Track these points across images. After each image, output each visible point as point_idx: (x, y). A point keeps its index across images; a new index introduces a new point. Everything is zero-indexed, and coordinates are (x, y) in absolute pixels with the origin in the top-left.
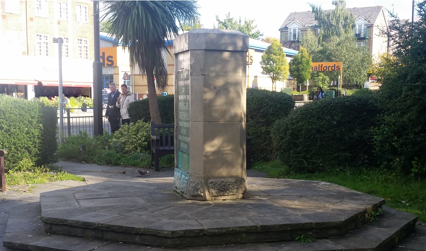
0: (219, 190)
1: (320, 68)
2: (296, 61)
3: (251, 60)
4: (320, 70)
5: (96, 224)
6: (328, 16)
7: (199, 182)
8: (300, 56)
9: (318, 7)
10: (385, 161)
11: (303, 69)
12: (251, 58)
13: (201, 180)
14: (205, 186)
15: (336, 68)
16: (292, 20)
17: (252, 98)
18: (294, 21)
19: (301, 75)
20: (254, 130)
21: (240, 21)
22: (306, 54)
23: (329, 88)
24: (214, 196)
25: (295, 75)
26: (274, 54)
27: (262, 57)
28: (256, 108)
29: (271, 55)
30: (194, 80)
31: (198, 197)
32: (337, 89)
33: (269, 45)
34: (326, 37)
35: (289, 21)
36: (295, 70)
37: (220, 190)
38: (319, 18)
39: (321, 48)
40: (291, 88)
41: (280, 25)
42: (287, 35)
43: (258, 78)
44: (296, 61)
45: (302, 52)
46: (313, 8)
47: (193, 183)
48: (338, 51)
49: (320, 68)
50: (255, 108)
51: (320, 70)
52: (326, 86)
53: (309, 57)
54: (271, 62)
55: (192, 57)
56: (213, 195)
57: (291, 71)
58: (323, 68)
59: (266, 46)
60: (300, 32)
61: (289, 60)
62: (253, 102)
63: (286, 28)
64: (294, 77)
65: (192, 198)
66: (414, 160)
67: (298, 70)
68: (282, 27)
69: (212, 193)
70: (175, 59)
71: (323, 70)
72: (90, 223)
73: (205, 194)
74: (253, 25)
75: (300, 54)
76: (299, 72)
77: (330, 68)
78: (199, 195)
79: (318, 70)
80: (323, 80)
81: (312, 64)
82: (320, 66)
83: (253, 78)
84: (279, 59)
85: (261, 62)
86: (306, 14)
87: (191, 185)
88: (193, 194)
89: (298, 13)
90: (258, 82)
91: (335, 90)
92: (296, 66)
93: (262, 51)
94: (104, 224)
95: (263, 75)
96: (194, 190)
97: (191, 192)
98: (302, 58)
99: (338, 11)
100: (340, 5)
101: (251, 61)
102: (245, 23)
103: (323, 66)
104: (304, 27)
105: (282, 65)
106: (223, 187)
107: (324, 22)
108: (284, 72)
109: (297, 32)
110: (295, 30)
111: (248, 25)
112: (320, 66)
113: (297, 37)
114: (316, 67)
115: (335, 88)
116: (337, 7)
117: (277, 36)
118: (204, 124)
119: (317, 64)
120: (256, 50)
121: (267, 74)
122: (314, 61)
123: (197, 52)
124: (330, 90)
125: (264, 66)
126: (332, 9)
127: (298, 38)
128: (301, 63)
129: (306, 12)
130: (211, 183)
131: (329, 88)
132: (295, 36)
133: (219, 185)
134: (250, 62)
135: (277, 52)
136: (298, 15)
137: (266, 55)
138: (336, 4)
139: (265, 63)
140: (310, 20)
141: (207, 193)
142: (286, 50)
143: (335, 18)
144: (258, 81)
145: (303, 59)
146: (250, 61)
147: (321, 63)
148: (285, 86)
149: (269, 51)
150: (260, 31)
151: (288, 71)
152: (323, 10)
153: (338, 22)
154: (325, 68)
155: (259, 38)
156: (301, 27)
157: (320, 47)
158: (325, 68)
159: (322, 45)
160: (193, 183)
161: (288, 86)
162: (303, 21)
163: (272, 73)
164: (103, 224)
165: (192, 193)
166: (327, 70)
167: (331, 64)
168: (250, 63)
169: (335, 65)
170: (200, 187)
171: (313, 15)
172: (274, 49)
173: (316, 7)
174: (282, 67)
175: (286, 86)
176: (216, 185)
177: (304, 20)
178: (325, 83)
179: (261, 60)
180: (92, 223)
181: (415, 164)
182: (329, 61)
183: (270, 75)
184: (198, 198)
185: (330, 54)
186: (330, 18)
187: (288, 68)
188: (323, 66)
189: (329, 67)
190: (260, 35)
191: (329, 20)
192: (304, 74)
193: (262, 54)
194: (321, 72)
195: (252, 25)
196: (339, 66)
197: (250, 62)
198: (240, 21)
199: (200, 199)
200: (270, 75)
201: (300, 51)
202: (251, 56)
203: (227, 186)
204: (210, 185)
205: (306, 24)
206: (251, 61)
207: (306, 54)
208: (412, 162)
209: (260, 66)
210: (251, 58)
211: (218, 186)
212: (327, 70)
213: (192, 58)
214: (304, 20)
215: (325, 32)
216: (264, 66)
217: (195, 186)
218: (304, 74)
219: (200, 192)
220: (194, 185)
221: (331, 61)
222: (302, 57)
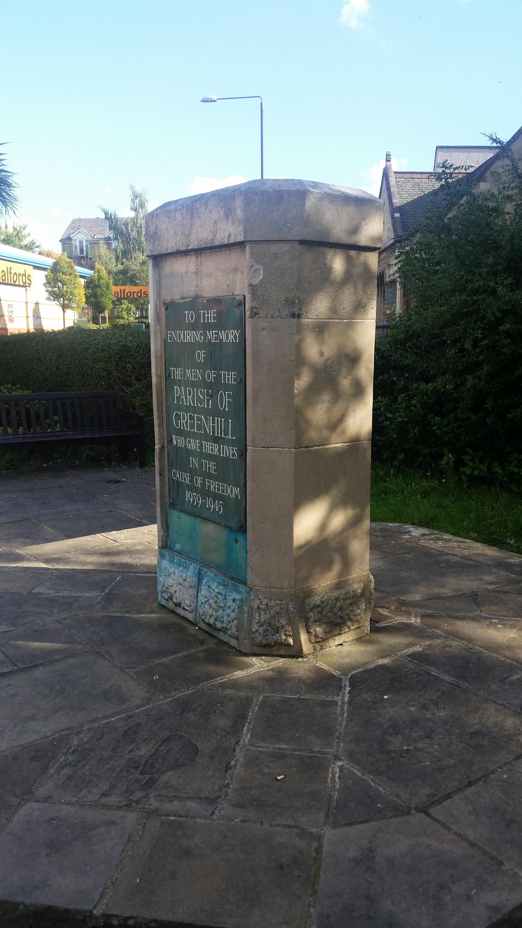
0: (330, 624)
1: (122, 293)
2: (92, 284)
3: (29, 280)
4: (122, 297)
5: (96, 918)
6: (126, 225)
7: (281, 609)
8: (96, 277)
9: (113, 213)
10: (401, 453)
11: (102, 295)
12: (29, 277)
13: (287, 604)
14: (300, 619)
15: (143, 295)
16: (76, 229)
17: (138, 346)
18: (79, 230)
19: (100, 302)
20: (143, 400)
21: (6, 227)
22: (104, 273)
23: (137, 321)
24: (320, 640)
25: (91, 302)
26: (63, 273)
27: (46, 276)
28: (145, 363)
29: (58, 274)
30: (265, 332)
31: (276, 647)
32: (147, 322)
33: (53, 261)
34: (125, 253)
35: (72, 229)
36: (91, 296)
37: (331, 622)
38: (115, 228)
39: (120, 267)
40: (85, 319)
41: (61, 234)
42: (72, 248)
43: (40, 305)
44: (92, 284)
45: (98, 272)
46: (106, 214)
47: (262, 613)
48: (143, 272)
49: (122, 293)
50: (144, 363)
51: (122, 297)
52: (132, 318)
53: (109, 279)
54: (59, 284)
55: (256, 262)
56: (317, 640)
57: (87, 297)
58: (125, 293)
59: (49, 262)
60: (89, 245)
61: (83, 281)
62: (139, 352)
63: (69, 239)
64: (91, 304)
65: (257, 650)
66: (467, 454)
67: (95, 296)
68: (63, 238)
69: (316, 634)
70: (154, 271)
71: (126, 297)
72: (67, 911)
73: (297, 640)
74: (25, 232)
75: (96, 274)
76: (97, 299)
77: (135, 294)
78: (281, 643)
79: (119, 297)
80: (128, 310)
81: (113, 288)
82: (122, 291)
83: (33, 306)
84: (71, 280)
85: (45, 284)
86: (95, 222)
87: (257, 618)
88: (264, 642)
89: (84, 220)
90: (40, 311)
91: (145, 323)
92: (92, 291)
93: (45, 269)
94: (134, 918)
95: (49, 302)
96: (266, 630)
97: (257, 634)
98: (99, 279)
99: (139, 220)
100: (141, 211)
101: (29, 282)
102: (14, 230)
103: (126, 291)
104: (93, 238)
105: (75, 288)
106: (340, 613)
107: (121, 233)
108: (78, 298)
109: (84, 245)
110: (81, 242)
111: (18, 233)
112: (122, 291)
113: (85, 252)
114: (116, 293)
115: (144, 320)
116: (137, 215)
117: (57, 249)
118: (295, 453)
119: (118, 289)
120: (35, 267)
121: (54, 300)
122: (116, 284)
123: (274, 248)
124: (139, 322)
125: (50, 289)
126: (130, 217)
127: (87, 253)
128: (99, 286)
129: (93, 219)
130: (312, 610)
131: (137, 321)
132: (82, 250)
133: (331, 611)
134: (28, 283)
135: (66, 270)
136: (83, 222)
137: (52, 274)
138: (135, 210)
139: (50, 285)
140: (100, 230)
141: (304, 637)
142: (79, 269)
143: (136, 229)
144: (40, 309)
145: (102, 281)
146: (27, 281)
147: (123, 288)
148: (77, 317)
149: (55, 269)
150: (35, 241)
151: (84, 297)
152: (119, 217)
153: (139, 233)
154: (129, 294)
155: (34, 250)
156: (90, 238)
157: (119, 266)
158: (129, 294)
159: (122, 264)
160: (262, 613)
161: (80, 317)
162: (91, 230)
163: (62, 299)
164: (128, 918)
165: (259, 639)
166: (132, 296)
167: (136, 289)
168: (27, 285)
169: (141, 290)
170: (284, 623)
171: (107, 224)
172: (62, 267)
173: (109, 212)
174: (76, 291)
175: (78, 317)
176: (323, 613)
177: (93, 229)
178: (130, 314)
179: (44, 281)
180: (78, 912)
181: (470, 461)
182: (133, 285)
183: (59, 301)
184: (278, 650)
185: (134, 276)
186: (129, 229)
187: (83, 292)
188: (126, 291)
189: (134, 293)
190: (36, 247)
191: (128, 231)
192: (104, 301)
193: (45, 273)
194: (124, 299)
195: (23, 233)
196: (147, 292)
197: (28, 283)
198: (6, 227)
199: (282, 652)
200: (59, 301)
201: (96, 270)
202: (29, 275)
203: (346, 610)
204: (311, 614)
205: (95, 235)
206: (29, 282)
207: (104, 273)
208: (463, 457)
209: (44, 288)
210: (29, 277)
211: (329, 614)
212: (132, 296)
213: (256, 266)
214: (93, 229)
215: (124, 247)
216: (50, 289)
217: (269, 619)
218: (104, 301)
219: (285, 634)
220: (267, 616)
221: (136, 284)
222: (100, 278)
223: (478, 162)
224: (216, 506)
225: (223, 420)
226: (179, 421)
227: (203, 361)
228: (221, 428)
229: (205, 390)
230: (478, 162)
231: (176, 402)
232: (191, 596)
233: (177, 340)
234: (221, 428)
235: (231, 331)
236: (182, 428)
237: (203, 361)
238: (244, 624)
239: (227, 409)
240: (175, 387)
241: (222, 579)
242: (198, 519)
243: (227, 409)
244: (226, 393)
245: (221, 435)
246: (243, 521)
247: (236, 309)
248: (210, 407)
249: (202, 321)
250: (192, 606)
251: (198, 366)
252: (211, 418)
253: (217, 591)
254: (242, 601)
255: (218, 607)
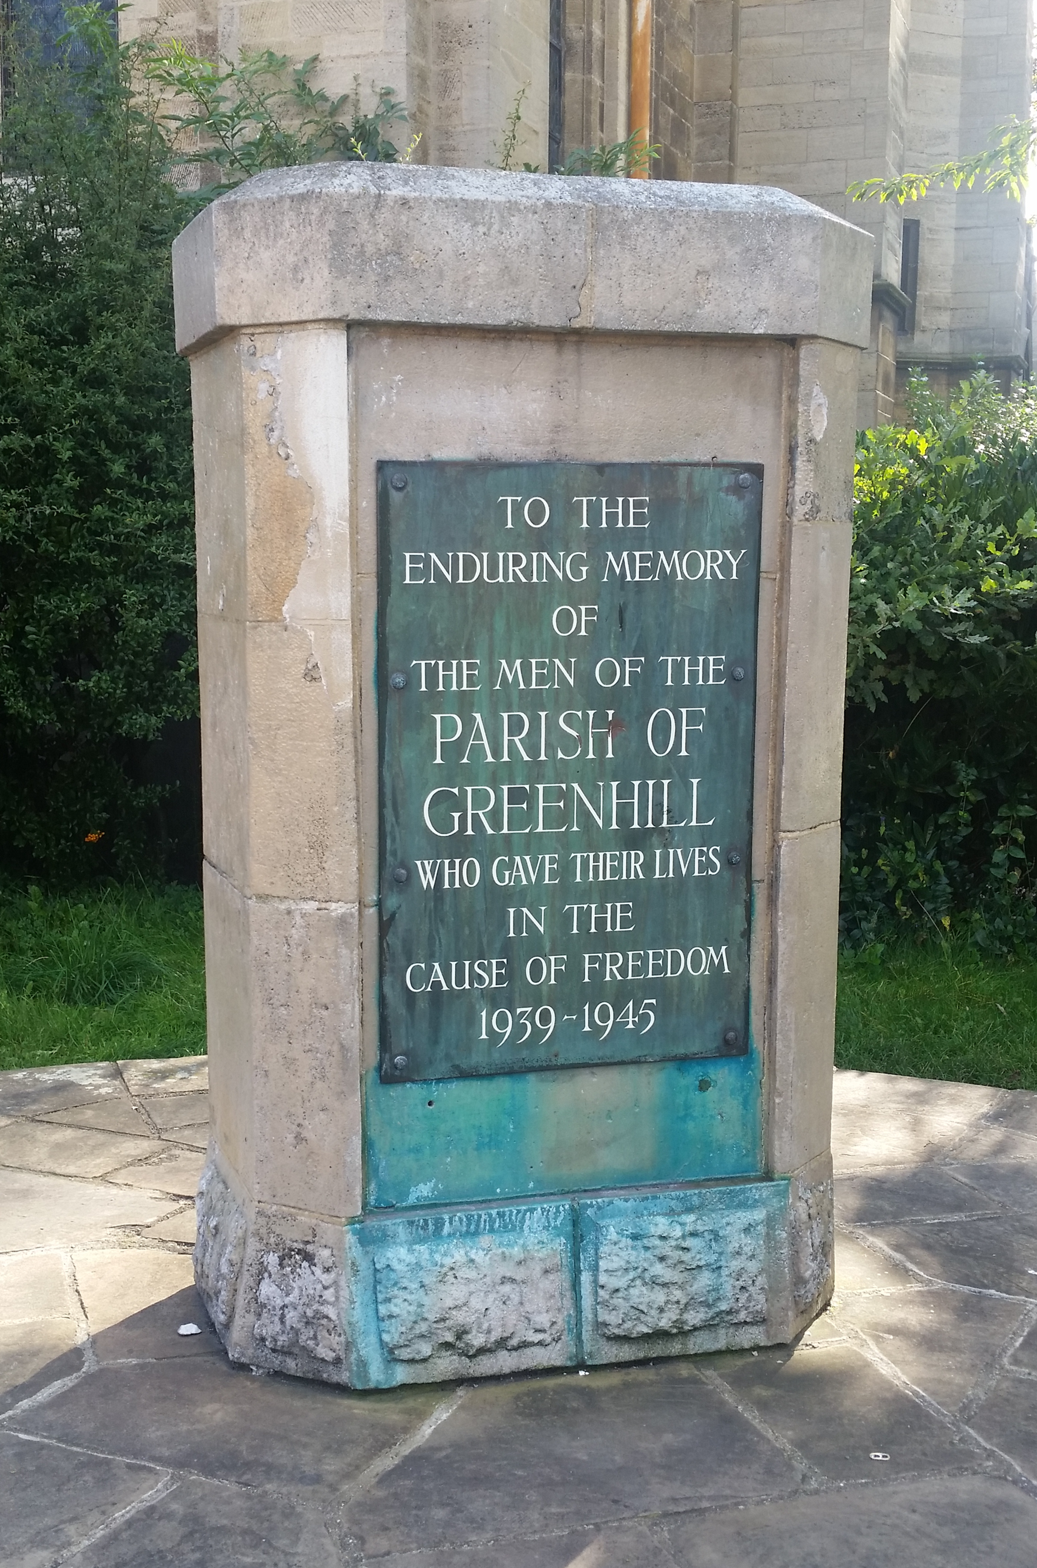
223: (125, 19)
224: (626, 1016)
225: (666, 782)
226: (456, 815)
227: (583, 633)
228: (658, 805)
229: (591, 713)
230: (125, 19)
231: (438, 760)
232: (552, 1296)
233: (455, 576)
234: (658, 805)
235: (709, 552)
236: (470, 832)
237: (583, 633)
238: (783, 1271)
239: (684, 753)
240: (438, 717)
241: (678, 1198)
242: (532, 1078)
243: (684, 753)
244: (684, 711)
245: (657, 821)
246: (739, 1024)
247: (733, 498)
248: (610, 755)
249: (585, 525)
250: (560, 1322)
251: (568, 647)
252: (614, 784)
253: (678, 1232)
254: (770, 1222)
255: (686, 1274)
